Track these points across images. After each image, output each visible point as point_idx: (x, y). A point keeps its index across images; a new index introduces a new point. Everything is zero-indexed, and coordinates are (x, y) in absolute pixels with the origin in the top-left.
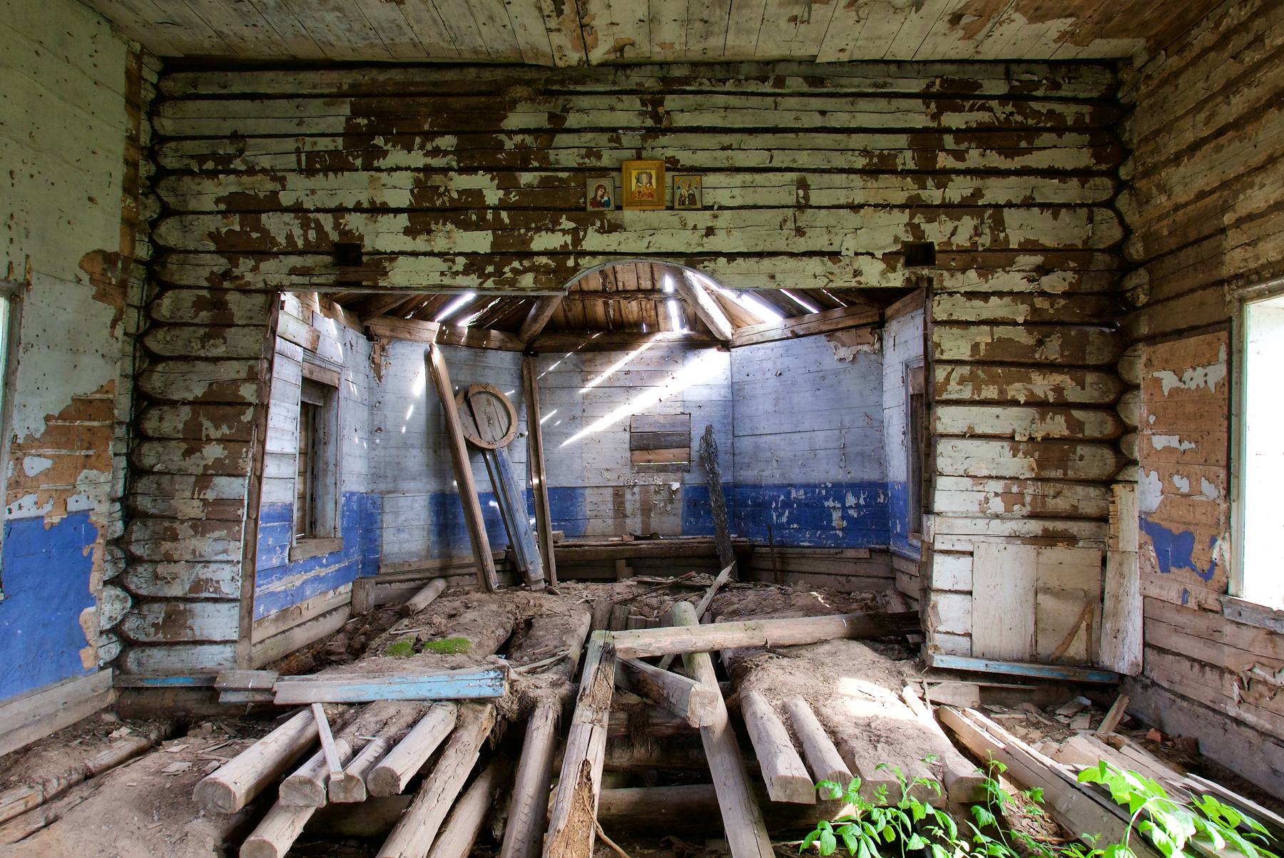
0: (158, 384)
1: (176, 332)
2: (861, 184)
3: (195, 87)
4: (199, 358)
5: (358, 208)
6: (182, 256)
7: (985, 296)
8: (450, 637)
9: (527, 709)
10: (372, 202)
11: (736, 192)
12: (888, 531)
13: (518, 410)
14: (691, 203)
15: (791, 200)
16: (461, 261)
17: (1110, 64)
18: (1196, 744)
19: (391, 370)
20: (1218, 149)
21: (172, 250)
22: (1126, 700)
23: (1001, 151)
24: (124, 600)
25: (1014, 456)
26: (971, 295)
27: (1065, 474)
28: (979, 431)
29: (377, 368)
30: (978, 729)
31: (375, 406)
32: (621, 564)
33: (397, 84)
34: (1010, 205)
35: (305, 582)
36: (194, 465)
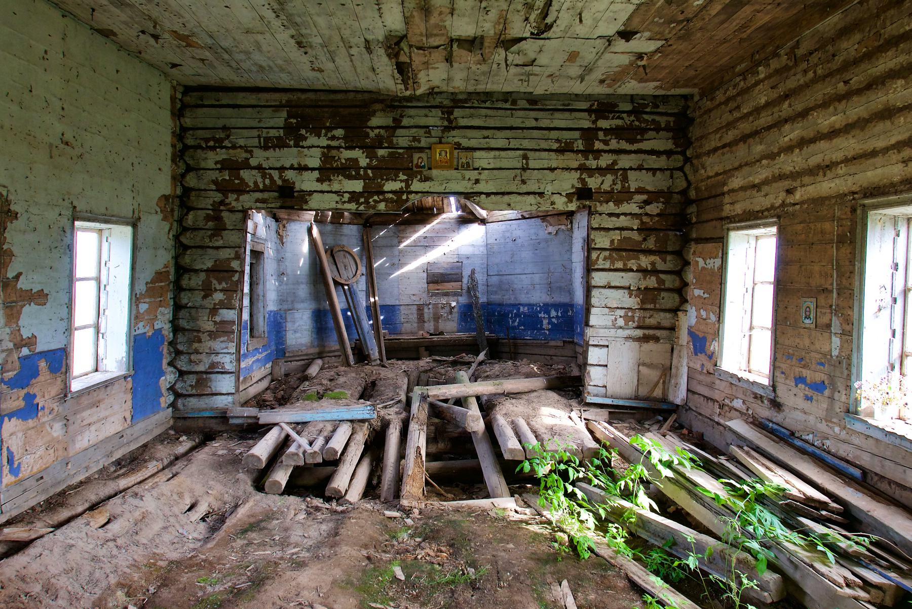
0: (188, 261)
1: (195, 233)
2: (555, 157)
3: (202, 101)
4: (209, 247)
5: (292, 168)
6: (197, 192)
7: (618, 215)
8: (335, 391)
9: (385, 425)
10: (299, 164)
11: (491, 161)
12: (573, 331)
13: (361, 259)
14: (467, 166)
15: (519, 165)
16: (347, 196)
17: (685, 97)
18: (702, 435)
19: (289, 239)
20: (723, 154)
21: (192, 189)
22: (676, 416)
23: (628, 141)
24: (175, 373)
25: (630, 297)
26: (611, 215)
27: (655, 306)
28: (613, 284)
29: (281, 238)
30: (604, 430)
31: (280, 260)
32: (422, 350)
33: (312, 100)
34: (631, 169)
35: (253, 362)
36: (209, 303)
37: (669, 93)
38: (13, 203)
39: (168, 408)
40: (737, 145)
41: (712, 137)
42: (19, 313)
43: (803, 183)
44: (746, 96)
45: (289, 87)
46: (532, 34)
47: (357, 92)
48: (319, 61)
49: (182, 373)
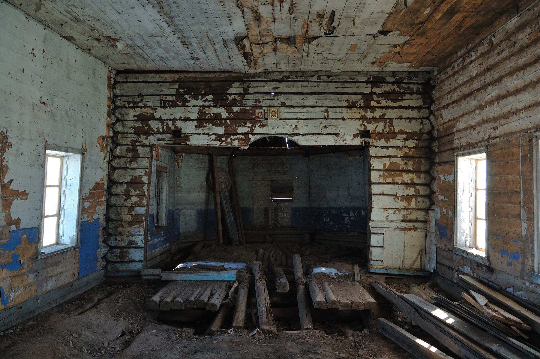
4: (128, 168)
5: (180, 119)
7: (387, 148)
10: (185, 117)
20: (453, 108)
21: (119, 133)
26: (382, 147)
28: (385, 193)
33: (193, 78)
36: (128, 203)
37: (418, 70)
38: (9, 138)
39: (102, 269)
40: (461, 101)
41: (446, 97)
42: (11, 204)
43: (500, 124)
44: (465, 71)
45: (179, 70)
46: (325, 33)
47: (221, 72)
48: (196, 53)
49: (111, 248)
